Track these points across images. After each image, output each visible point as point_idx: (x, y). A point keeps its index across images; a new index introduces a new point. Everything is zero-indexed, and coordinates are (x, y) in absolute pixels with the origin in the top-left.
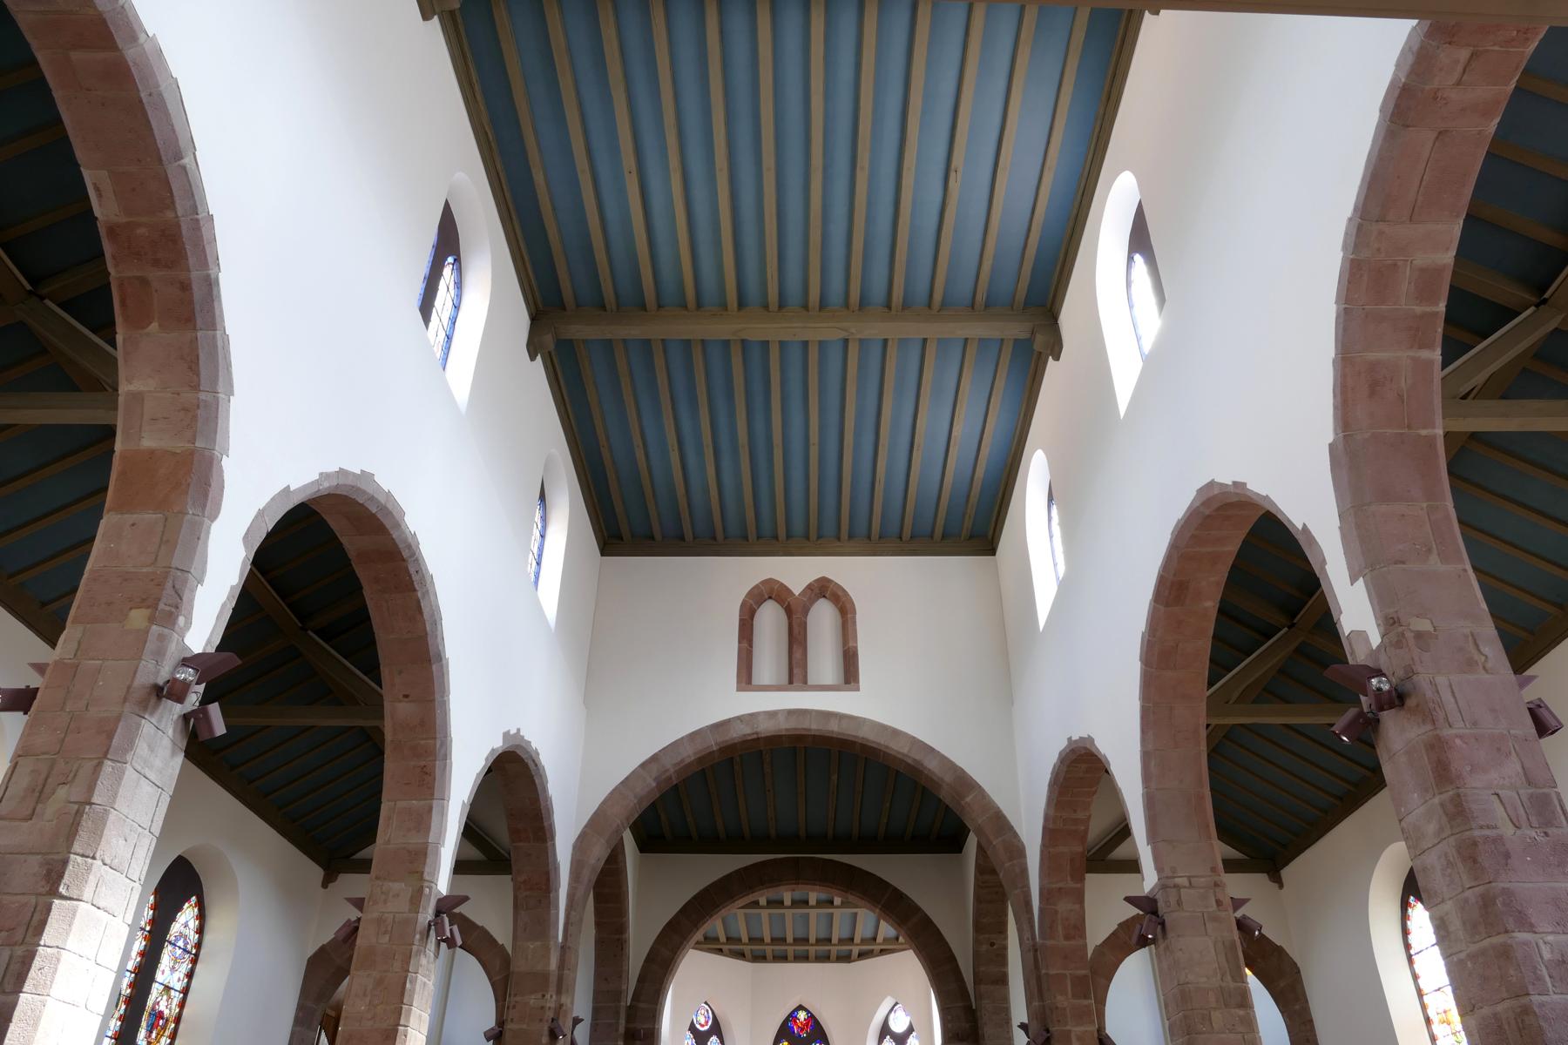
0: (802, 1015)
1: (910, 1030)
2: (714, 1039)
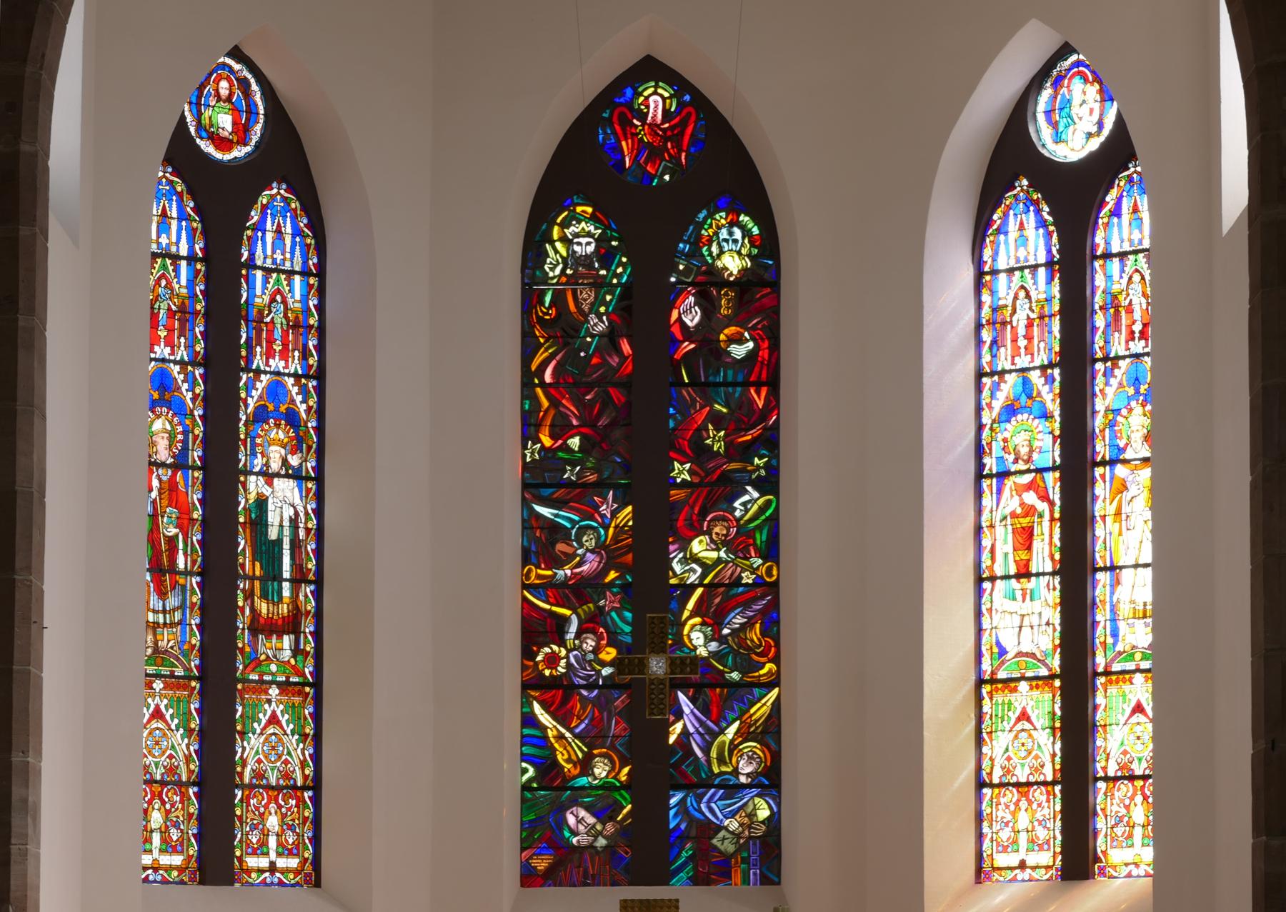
0: (655, 101)
1: (1117, 153)
2: (275, 193)
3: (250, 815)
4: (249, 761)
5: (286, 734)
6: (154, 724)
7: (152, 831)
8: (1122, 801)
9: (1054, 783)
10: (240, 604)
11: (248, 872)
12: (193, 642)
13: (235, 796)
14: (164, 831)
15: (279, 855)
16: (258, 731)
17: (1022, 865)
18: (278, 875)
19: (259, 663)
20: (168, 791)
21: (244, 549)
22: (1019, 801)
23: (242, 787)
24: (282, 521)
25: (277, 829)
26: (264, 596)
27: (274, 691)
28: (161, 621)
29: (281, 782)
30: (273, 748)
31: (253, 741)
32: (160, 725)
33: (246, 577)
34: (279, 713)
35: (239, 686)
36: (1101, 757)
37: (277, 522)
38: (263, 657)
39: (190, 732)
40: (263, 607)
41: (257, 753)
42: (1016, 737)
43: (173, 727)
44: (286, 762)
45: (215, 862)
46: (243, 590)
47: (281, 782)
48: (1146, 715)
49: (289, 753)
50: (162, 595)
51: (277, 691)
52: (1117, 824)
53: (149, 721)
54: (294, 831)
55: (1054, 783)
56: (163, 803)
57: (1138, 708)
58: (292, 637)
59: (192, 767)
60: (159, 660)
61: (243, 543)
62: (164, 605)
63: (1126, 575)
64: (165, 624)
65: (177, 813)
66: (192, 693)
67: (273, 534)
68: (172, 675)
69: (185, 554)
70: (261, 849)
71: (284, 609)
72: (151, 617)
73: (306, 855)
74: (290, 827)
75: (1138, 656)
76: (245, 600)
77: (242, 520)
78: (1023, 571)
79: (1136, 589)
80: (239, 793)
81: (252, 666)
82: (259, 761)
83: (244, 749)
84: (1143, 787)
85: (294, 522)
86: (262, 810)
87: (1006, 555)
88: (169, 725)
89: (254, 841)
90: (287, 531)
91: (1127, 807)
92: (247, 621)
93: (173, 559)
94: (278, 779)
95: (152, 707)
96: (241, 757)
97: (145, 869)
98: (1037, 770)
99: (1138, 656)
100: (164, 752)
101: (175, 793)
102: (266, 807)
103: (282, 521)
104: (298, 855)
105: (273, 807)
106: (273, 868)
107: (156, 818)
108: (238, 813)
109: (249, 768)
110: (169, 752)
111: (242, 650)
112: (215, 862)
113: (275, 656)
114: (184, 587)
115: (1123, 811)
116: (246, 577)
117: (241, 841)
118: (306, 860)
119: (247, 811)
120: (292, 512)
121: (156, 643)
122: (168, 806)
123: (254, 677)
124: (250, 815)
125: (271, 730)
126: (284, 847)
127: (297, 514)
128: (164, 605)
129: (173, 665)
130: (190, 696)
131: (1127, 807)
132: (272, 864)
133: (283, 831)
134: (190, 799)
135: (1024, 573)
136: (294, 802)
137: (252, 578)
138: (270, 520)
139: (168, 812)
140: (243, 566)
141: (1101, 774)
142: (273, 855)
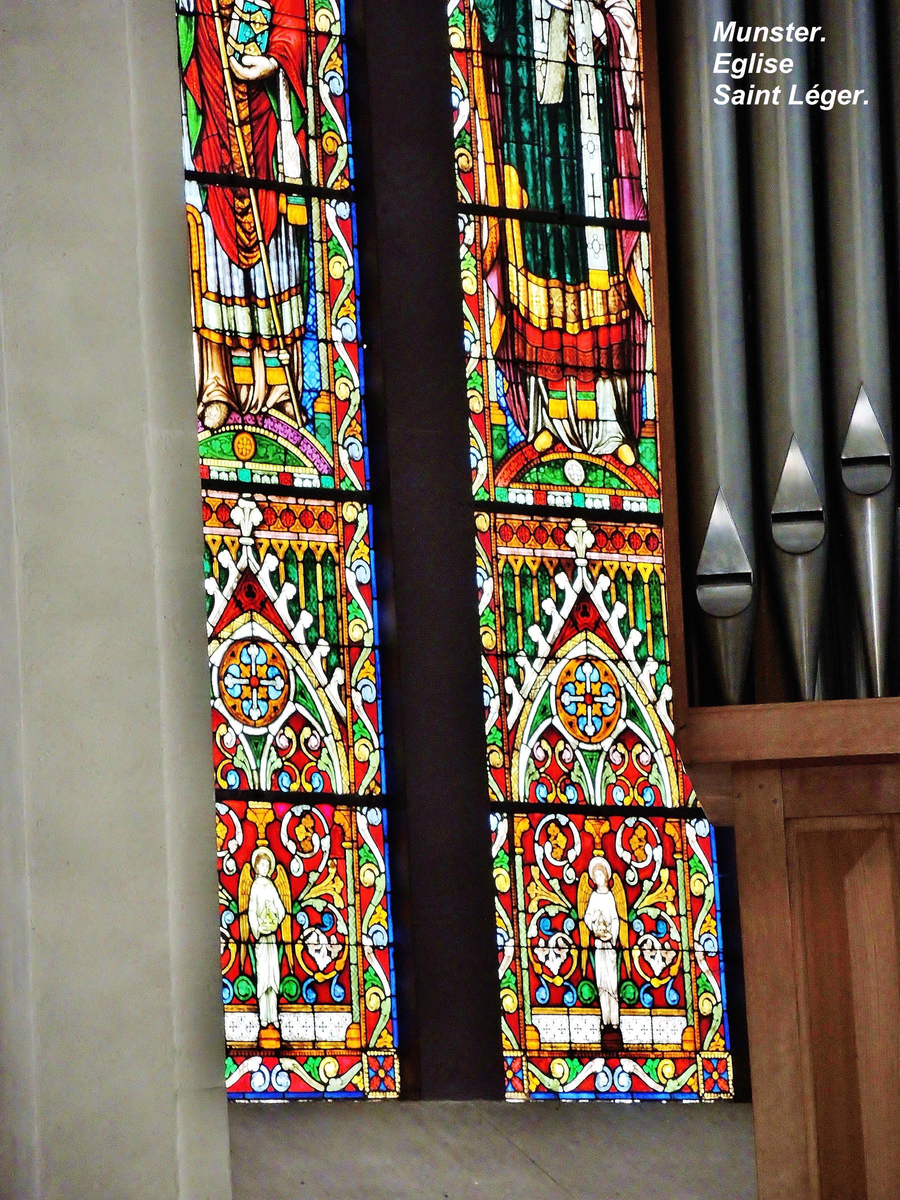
3: (537, 891)
4: (523, 734)
5: (622, 658)
6: (242, 627)
7: (252, 942)
10: (469, 285)
11: (543, 1060)
12: (342, 392)
13: (488, 836)
15: (627, 1005)
16: (544, 650)
18: (628, 1065)
19: (535, 460)
20: (296, 821)
21: (469, 129)
23: (510, 808)
24: (571, 51)
25: (616, 930)
26: (537, 267)
27: (580, 537)
28: (244, 327)
29: (542, 792)
30: (589, 699)
31: (529, 678)
32: (261, 628)
33: (479, 210)
34: (597, 598)
35: (482, 522)
37: (558, 50)
38: (543, 442)
39: (343, 652)
40: (535, 297)
41: (544, 712)
44: (627, 738)
45: (448, 1030)
46: (476, 248)
47: (618, 796)
49: (633, 714)
50: (240, 252)
51: (589, 539)
53: (226, 620)
54: (666, 938)
56: (283, 859)
58: (622, 384)
59: (361, 752)
60: (245, 444)
61: (464, 108)
62: (248, 282)
64: (255, 336)
65: (326, 887)
66: (348, 537)
67: (549, 88)
68: (285, 488)
69: (301, 133)
70: (574, 987)
71: (596, 307)
72: (212, 315)
73: (705, 1008)
74: (652, 926)
76: (484, 275)
77: (457, 40)
80: (498, 824)
81: (513, 465)
82: (552, 735)
83: (506, 701)
84: (273, 827)
85: (607, 54)
86: (570, 875)
88: (286, 632)
89: (554, 965)
90: (588, 81)
91: (570, 891)
92: (494, 335)
93: (265, 151)
94: (609, 788)
96: (501, 724)
97: (240, 1054)
100: (277, 711)
101: (316, 828)
102: (581, 866)
103: (571, 51)
104: (681, 1005)
105: (599, 868)
106: (612, 1045)
107: (265, 903)
108: (502, 884)
109: (525, 752)
110: (290, 709)
111: (482, 418)
112: (448, 1030)
113: (576, 440)
114: (303, 234)
116: (479, 210)
117: (514, 968)
118: (706, 1020)
119: (528, 879)
120: (599, 24)
121: (232, 391)
122: (297, 867)
123: (522, 496)
124: (537, 891)
125: (577, 647)
126: (639, 983)
127: (612, 30)
128: (248, 282)
129: (286, 458)
130: (343, 547)
131: (570, 891)
132: (611, 1033)
133: (634, 936)
134: (359, 844)
136: (658, 853)
137: (502, 213)
138: (539, 46)
139: (297, 885)
140: (469, 175)
142: (610, 1008)
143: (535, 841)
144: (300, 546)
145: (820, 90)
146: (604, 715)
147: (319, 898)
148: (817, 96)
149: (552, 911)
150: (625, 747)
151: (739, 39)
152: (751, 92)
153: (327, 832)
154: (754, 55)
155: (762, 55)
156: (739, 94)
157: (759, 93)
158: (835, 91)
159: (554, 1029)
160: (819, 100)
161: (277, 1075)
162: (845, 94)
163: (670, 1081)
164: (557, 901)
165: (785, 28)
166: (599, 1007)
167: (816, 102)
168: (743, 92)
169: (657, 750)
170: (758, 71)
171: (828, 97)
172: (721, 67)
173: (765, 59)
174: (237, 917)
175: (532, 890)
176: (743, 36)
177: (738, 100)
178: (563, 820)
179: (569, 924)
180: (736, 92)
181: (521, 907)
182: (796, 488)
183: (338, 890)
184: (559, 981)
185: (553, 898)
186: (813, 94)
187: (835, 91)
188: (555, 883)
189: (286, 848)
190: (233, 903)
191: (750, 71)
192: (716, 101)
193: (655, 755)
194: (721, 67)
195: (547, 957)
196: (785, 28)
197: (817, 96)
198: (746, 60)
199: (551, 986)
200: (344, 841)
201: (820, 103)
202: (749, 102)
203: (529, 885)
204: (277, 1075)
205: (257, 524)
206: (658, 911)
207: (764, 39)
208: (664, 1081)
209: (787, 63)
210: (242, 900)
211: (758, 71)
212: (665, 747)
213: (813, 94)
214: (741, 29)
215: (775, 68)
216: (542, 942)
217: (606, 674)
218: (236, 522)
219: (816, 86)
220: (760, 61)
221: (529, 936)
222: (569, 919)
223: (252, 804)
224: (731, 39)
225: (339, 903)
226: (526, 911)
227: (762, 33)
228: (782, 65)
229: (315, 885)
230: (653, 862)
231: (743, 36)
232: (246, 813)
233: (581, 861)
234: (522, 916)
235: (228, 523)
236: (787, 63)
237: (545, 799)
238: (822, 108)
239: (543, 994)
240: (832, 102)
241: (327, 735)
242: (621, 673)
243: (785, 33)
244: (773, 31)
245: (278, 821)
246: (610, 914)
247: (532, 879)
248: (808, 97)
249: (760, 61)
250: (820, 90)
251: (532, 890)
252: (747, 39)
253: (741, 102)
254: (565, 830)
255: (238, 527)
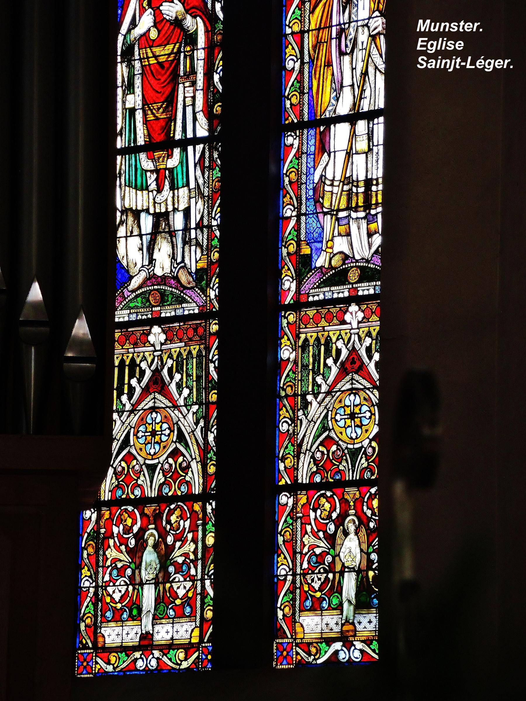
5: (176, 406)
8: (322, 528)
9: (204, 498)
14: (162, 579)
17: (146, 643)
22: (143, 530)
36: (286, 449)
42: (142, 421)
43: (181, 402)
47: (166, 490)
48: (368, 377)
52: (312, 570)
55: (204, 498)
57: (353, 365)
63: (340, 134)
75: (353, 276)
78: (159, 138)
79: (354, 156)
84: (359, 502)
87: (132, 111)
91: (331, 539)
95: (344, 353)
98: (175, 476)
99: (353, 276)
102: (340, 521)
106: (146, 643)
115: (322, 545)
131: (331, 539)
135: (162, 142)
141: (285, 480)
143: (310, 509)
144: (323, 335)
145: (485, 60)
146: (162, 441)
147: (181, 556)
148: (483, 63)
149: (318, 551)
150: (126, 463)
151: (432, 30)
152: (439, 61)
153: (189, 516)
154: (441, 39)
155: (445, 39)
156: (432, 62)
157: (444, 61)
158: (493, 60)
159: (113, 636)
160: (484, 65)
161: (353, 652)
162: (499, 62)
163: (339, 649)
164: (322, 544)
165: (459, 24)
166: (141, 620)
167: (482, 67)
168: (434, 61)
169: (193, 459)
170: (443, 48)
171: (489, 64)
172: (421, 46)
173: (447, 41)
174: (334, 558)
175: (306, 539)
176: (434, 28)
177: (431, 65)
178: (130, 508)
179: (329, 558)
180: (430, 61)
181: (298, 550)
182: (35, 305)
183: (192, 550)
184: (119, 606)
185: (122, 557)
186: (481, 62)
187: (493, 60)
188: (123, 548)
189: (365, 513)
190: (331, 550)
191: (439, 48)
192: (418, 66)
193: (192, 463)
194: (421, 46)
195: (313, 580)
196: (459, 24)
197: (483, 63)
198: (436, 42)
199: (115, 610)
200: (350, 510)
201: (485, 67)
202: (438, 67)
203: (304, 536)
204: (353, 652)
205: (360, 320)
206: (183, 558)
207: (447, 30)
208: (179, 662)
209: (460, 44)
210: (338, 548)
211: (443, 48)
212: (198, 457)
213: (481, 62)
214: (433, 24)
215: (453, 47)
216: (111, 584)
217: (166, 417)
218: (348, 321)
219: (482, 57)
220: (444, 42)
221: (104, 581)
222: (329, 556)
223: (347, 489)
224: (427, 30)
225: (192, 557)
226: (301, 553)
227: (445, 26)
228: (457, 45)
229: (180, 548)
230: (184, 529)
231: (434, 28)
232: (343, 495)
233: (141, 534)
234: (298, 556)
235: (344, 322)
236: (460, 44)
237: (167, 494)
238: (486, 70)
239: (308, 603)
240: (492, 67)
241: (310, 450)
242: (175, 414)
243: (458, 26)
244: (452, 25)
245: (362, 497)
246: (356, 551)
247: (306, 533)
248: (478, 63)
249: (444, 43)
250: (485, 60)
251: (306, 539)
252: (436, 30)
253: (433, 67)
254: (131, 515)
255: (350, 323)
